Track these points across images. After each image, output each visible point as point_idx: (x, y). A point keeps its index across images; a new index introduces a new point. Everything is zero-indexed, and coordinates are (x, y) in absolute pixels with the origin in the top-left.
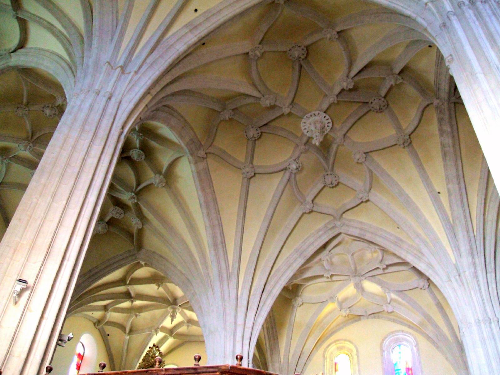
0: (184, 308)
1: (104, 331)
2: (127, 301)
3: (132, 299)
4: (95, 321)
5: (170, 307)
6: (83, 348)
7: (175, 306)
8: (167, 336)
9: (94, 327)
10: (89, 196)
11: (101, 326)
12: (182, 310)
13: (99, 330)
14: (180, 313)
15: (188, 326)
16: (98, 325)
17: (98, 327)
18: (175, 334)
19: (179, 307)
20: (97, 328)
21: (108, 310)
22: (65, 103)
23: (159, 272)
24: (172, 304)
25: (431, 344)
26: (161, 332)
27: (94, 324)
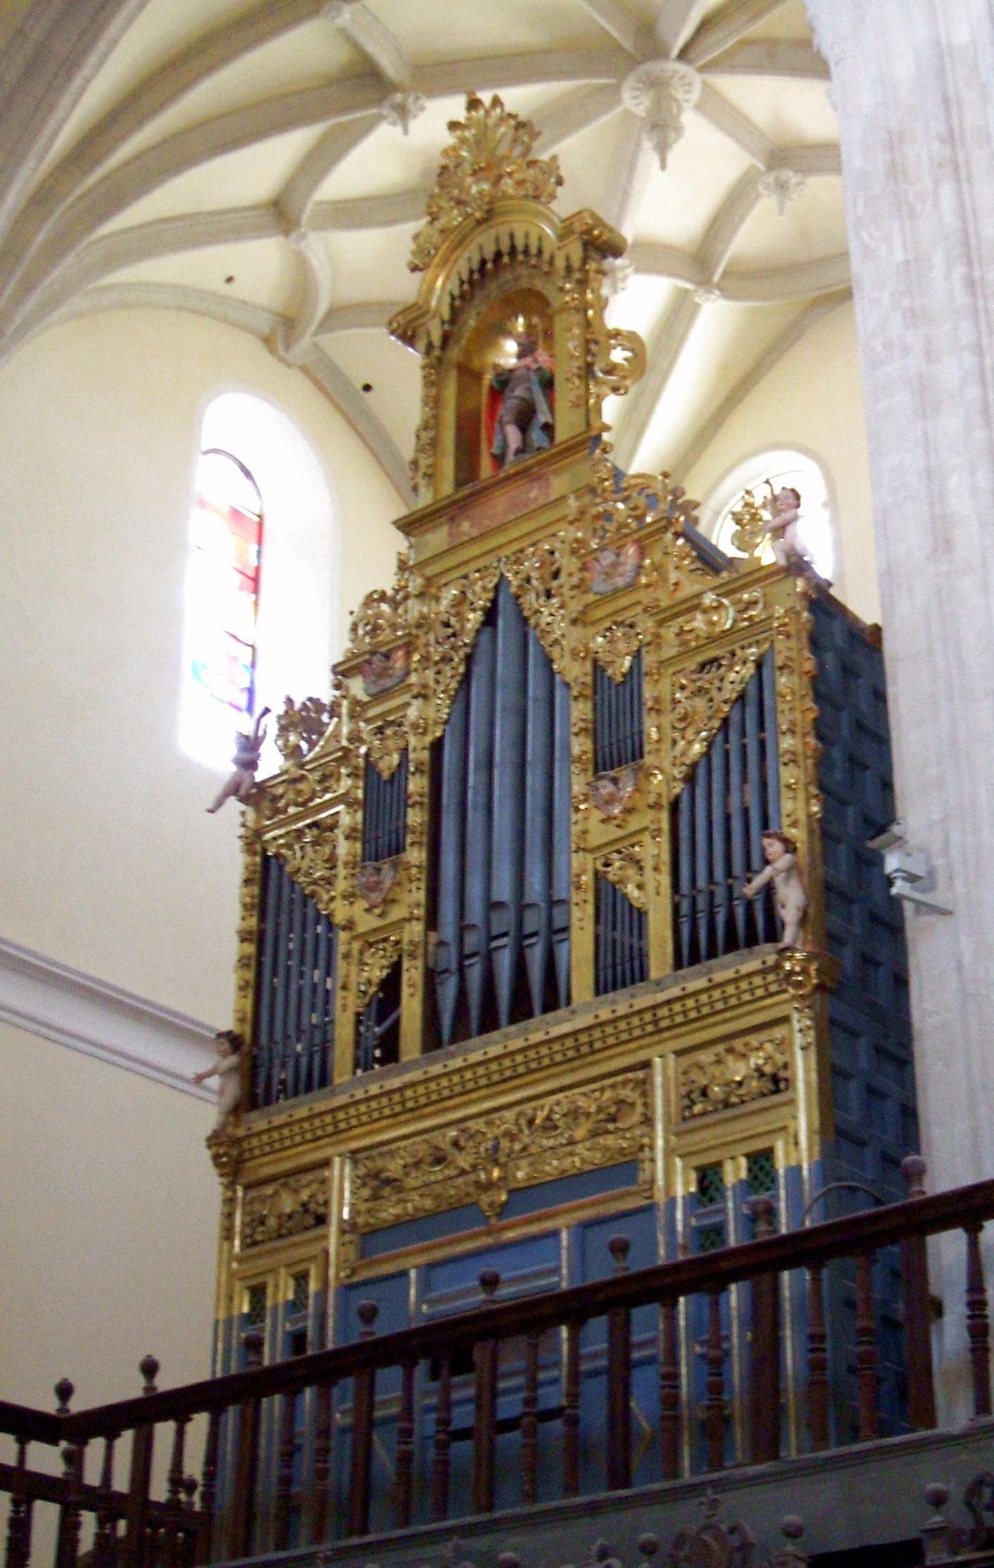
0: (725, 64)
1: (335, 371)
2: (380, 118)
3: (398, 97)
4: (264, 325)
5: (631, 81)
6: (249, 483)
7: (654, 67)
8: (686, 292)
9: (272, 360)
10: (495, 871)
11: (305, 342)
12: (708, 90)
13: (304, 369)
14: (698, 107)
15: (782, 187)
16: (288, 347)
17: (290, 356)
18: (726, 274)
19: (681, 68)
20: (289, 365)
21: (297, 224)
22: (610, 1103)
23: (533, 1269)
24: (634, 62)
25: (866, 722)
26: (638, 270)
27: (268, 341)
